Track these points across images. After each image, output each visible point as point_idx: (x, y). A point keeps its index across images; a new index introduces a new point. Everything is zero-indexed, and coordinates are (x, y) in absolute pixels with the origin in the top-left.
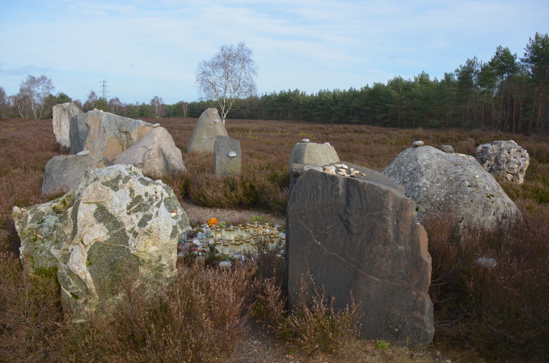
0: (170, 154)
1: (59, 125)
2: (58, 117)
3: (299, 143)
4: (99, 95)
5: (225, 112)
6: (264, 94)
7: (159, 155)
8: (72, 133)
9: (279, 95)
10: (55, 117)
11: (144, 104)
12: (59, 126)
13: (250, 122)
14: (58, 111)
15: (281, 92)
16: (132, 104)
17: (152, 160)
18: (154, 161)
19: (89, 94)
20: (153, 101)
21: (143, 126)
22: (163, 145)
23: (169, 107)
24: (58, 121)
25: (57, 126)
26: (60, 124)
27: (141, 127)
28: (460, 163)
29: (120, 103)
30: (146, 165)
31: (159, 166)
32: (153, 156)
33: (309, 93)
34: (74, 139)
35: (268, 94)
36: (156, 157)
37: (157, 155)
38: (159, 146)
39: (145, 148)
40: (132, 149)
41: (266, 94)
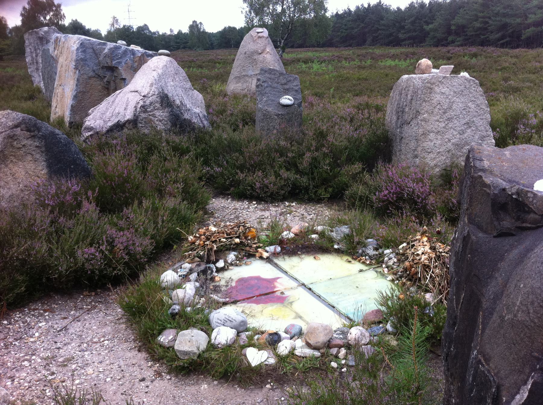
0: (182, 103)
1: (35, 61)
2: (32, 50)
3: (406, 76)
4: (123, 23)
5: (457, 308)
6: (335, 13)
7: (161, 106)
8: (45, 72)
9: (355, 12)
10: (29, 50)
11: (180, 33)
12: (35, 64)
13: (316, 51)
14: (32, 41)
15: (358, 7)
16: (165, 33)
17: (150, 115)
18: (154, 115)
19: (111, 21)
20: (191, 27)
21: (140, 57)
22: (169, 88)
23: (204, 32)
24: (34, 55)
25: (33, 63)
26: (36, 60)
27: (137, 59)
28: (220, 61)
29: (150, 32)
30: (141, 123)
31: (165, 125)
32: (152, 108)
33: (394, 7)
34: (48, 82)
35: (339, 13)
36: (157, 109)
37: (158, 105)
38: (161, 90)
39: (136, 93)
40: (117, 96)
41: (337, 12)
